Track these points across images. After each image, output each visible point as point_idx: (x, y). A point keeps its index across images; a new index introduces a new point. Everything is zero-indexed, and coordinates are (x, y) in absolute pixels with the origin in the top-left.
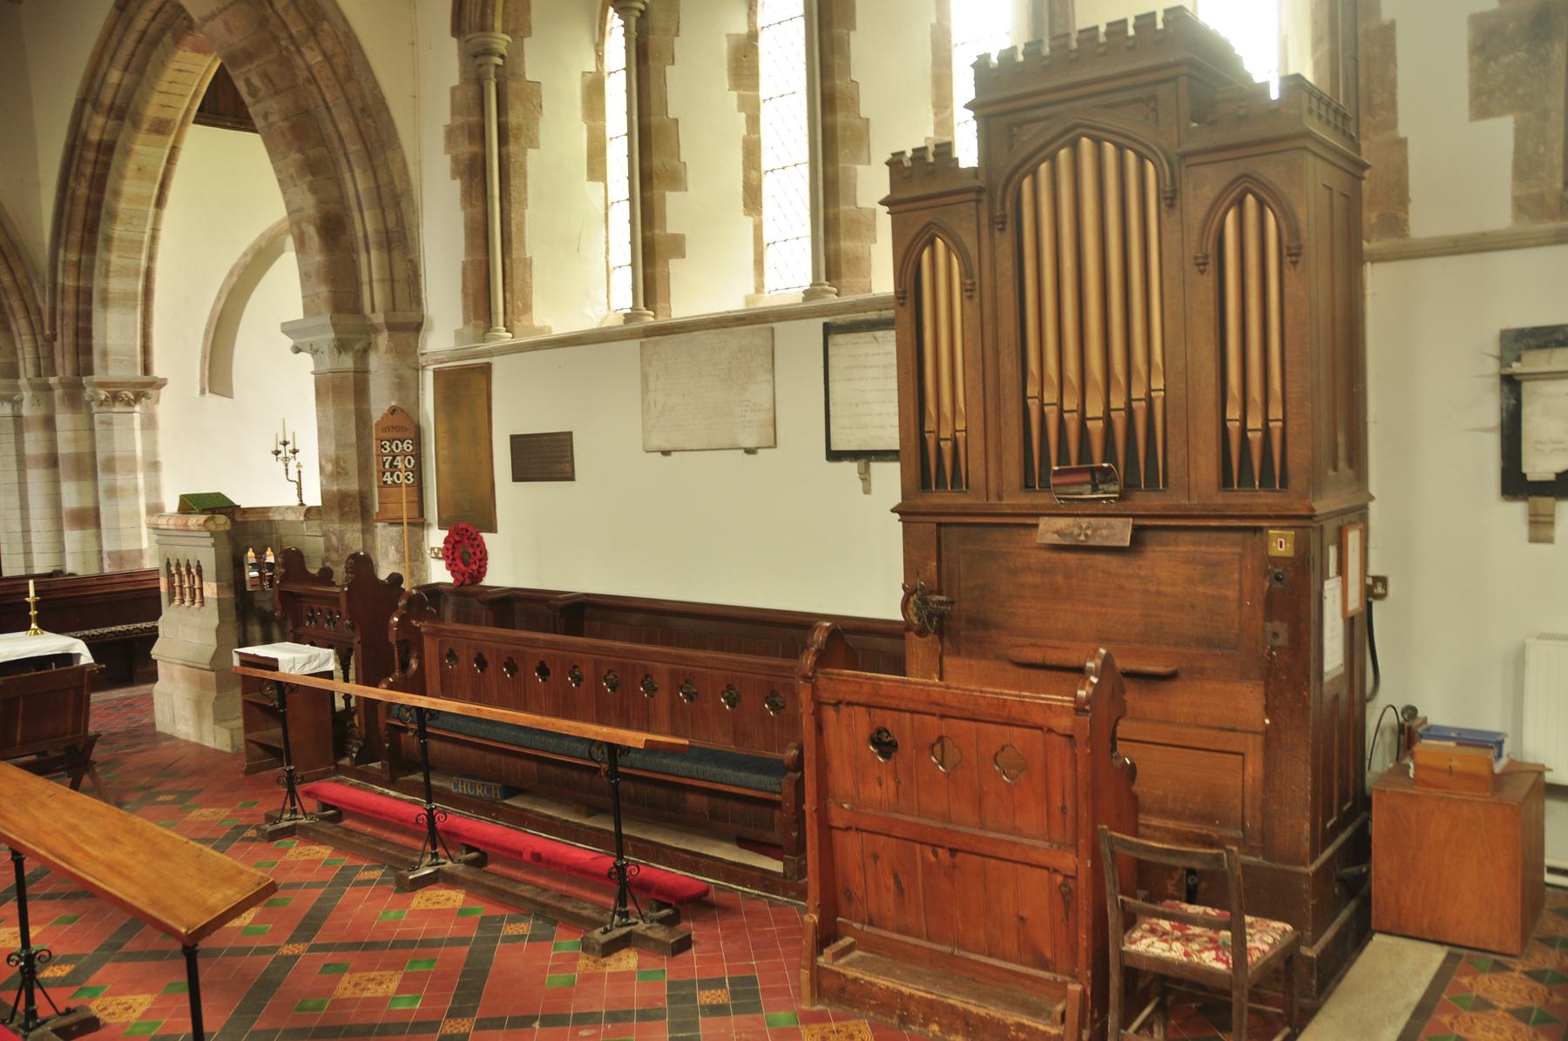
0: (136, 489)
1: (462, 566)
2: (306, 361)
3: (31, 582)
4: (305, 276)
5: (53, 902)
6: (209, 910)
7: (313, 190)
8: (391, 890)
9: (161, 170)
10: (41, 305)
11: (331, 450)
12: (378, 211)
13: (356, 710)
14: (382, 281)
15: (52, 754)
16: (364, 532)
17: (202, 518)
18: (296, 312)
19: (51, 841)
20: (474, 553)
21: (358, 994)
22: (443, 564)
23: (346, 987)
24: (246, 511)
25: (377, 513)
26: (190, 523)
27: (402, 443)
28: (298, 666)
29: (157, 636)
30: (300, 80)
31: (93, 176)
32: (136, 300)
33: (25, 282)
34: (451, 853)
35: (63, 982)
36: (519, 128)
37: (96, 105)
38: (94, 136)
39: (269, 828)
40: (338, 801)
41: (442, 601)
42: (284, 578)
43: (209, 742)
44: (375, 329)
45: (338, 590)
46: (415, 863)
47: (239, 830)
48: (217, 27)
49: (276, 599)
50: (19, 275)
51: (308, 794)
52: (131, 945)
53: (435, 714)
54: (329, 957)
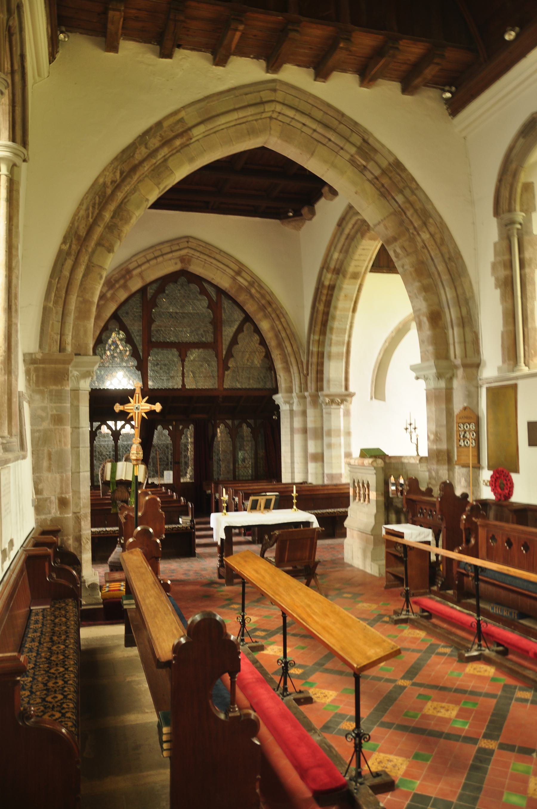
0: (340, 445)
1: (500, 490)
2: (422, 383)
3: (294, 487)
4: (422, 342)
5: (296, 638)
6: (368, 658)
7: (426, 300)
8: (455, 660)
9: (355, 296)
10: (303, 360)
11: (433, 428)
12: (458, 308)
13: (441, 562)
14: (460, 343)
15: (299, 567)
16: (449, 470)
17: (370, 460)
18: (417, 359)
19: (299, 611)
20: (507, 484)
21: (435, 713)
22: (489, 489)
23: (429, 708)
24: (390, 458)
25: (456, 462)
26: (365, 463)
27: (469, 425)
28: (414, 537)
29: (347, 516)
30: (419, 248)
31: (326, 300)
32: (343, 356)
33: (297, 350)
34: (489, 645)
35: (299, 677)
36: (531, 259)
37: (328, 269)
38: (327, 283)
39: (395, 617)
40: (431, 609)
41: (488, 508)
42: (409, 492)
43: (368, 570)
44: (456, 367)
45: (435, 499)
46: (469, 648)
47: (381, 616)
48: (381, 228)
49: (404, 501)
50: (295, 347)
51: (416, 603)
52: (329, 665)
53: (484, 570)
54: (421, 690)
